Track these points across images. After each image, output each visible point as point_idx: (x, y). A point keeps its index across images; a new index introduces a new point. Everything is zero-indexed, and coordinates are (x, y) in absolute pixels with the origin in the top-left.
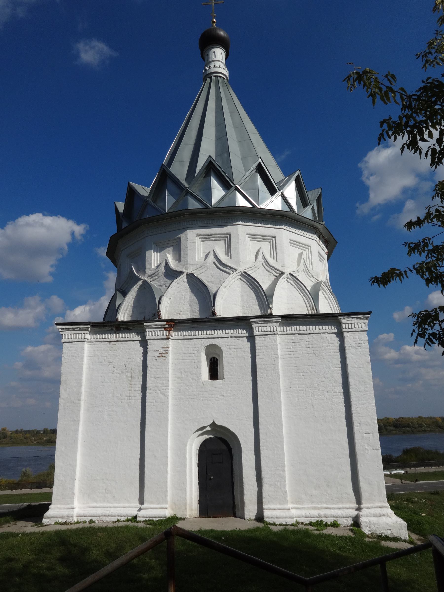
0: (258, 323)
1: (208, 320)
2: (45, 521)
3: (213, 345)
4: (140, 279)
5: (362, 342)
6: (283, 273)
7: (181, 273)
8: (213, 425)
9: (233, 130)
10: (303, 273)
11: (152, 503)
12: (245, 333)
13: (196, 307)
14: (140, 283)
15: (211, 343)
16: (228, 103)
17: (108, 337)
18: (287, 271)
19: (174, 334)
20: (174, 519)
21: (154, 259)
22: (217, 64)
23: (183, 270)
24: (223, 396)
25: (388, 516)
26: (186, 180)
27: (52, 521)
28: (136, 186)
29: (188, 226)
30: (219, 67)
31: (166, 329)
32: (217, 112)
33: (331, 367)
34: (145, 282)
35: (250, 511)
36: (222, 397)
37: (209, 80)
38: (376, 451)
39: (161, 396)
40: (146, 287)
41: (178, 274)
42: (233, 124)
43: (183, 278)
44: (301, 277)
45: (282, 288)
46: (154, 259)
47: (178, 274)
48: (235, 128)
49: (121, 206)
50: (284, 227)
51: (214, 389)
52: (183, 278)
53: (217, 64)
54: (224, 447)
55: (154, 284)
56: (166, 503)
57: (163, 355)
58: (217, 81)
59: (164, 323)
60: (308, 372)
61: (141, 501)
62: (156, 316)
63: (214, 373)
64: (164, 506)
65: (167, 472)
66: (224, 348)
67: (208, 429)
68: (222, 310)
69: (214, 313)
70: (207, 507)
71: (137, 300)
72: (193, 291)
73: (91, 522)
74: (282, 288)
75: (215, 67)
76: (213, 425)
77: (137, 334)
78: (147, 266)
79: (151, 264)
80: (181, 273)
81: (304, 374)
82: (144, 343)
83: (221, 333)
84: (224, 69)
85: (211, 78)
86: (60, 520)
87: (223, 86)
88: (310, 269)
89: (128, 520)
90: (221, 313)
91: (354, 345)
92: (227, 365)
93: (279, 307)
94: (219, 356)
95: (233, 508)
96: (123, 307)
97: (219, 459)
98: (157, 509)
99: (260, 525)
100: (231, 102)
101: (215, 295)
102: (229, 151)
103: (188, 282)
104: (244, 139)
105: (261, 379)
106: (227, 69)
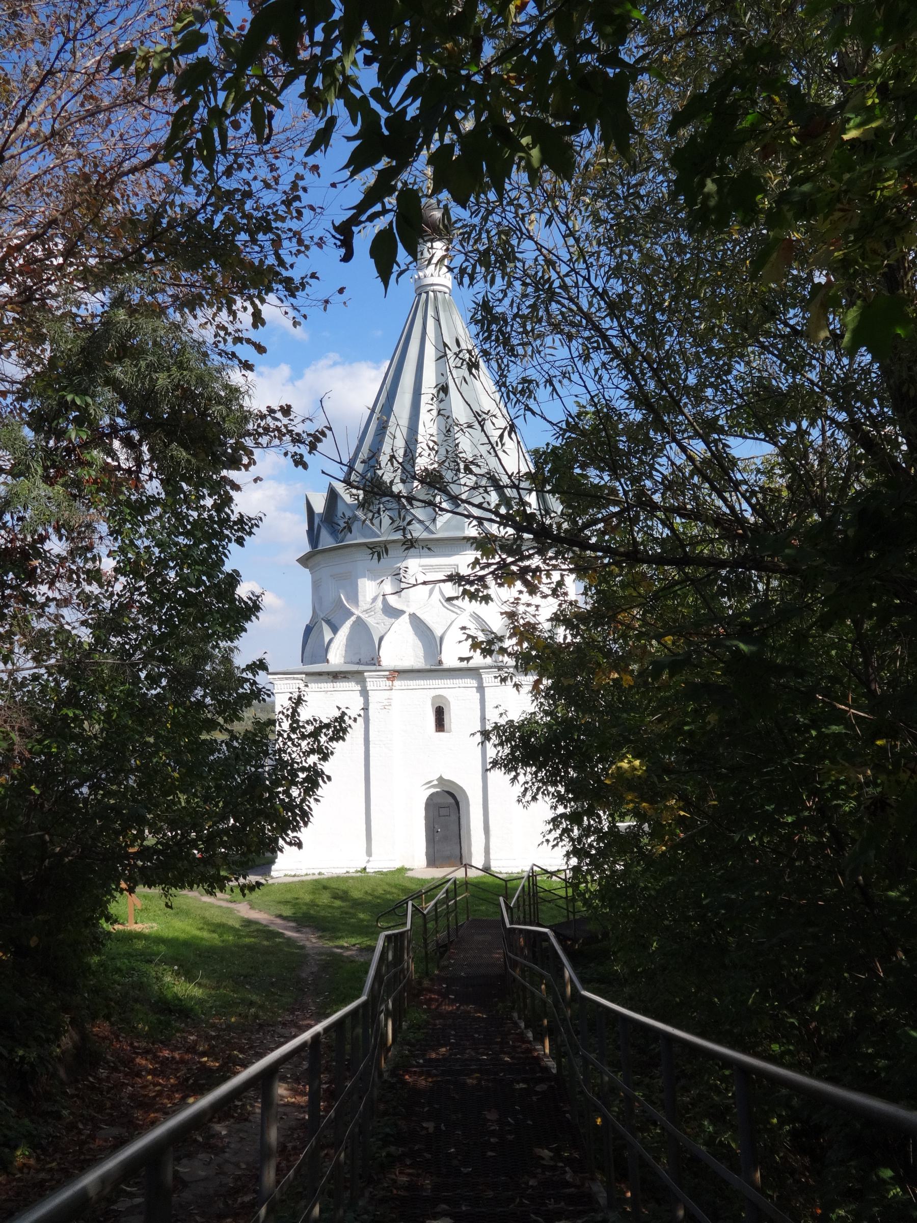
0: (488, 673)
1: (435, 670)
2: (272, 874)
3: (439, 696)
4: (353, 614)
7: (403, 612)
8: (441, 779)
12: (474, 683)
13: (421, 653)
14: (353, 618)
17: (323, 685)
19: (397, 683)
20: (402, 870)
21: (368, 588)
23: (404, 609)
27: (281, 874)
29: (498, 881)
34: (359, 618)
35: (478, 860)
37: (424, 296)
40: (361, 626)
41: (400, 613)
43: (405, 618)
46: (368, 588)
47: (400, 613)
52: (405, 618)
54: (452, 801)
55: (370, 621)
58: (436, 297)
61: (369, 853)
62: (375, 661)
63: (440, 725)
67: (436, 782)
69: (440, 663)
70: (433, 860)
71: (350, 639)
72: (416, 634)
73: (320, 874)
76: (441, 779)
77: (357, 683)
78: (360, 598)
79: (365, 596)
80: (403, 612)
82: (365, 693)
83: (449, 683)
85: (427, 293)
86: (289, 873)
89: (357, 872)
92: (453, 718)
95: (461, 860)
96: (333, 646)
98: (384, 860)
101: (442, 639)
103: (411, 622)
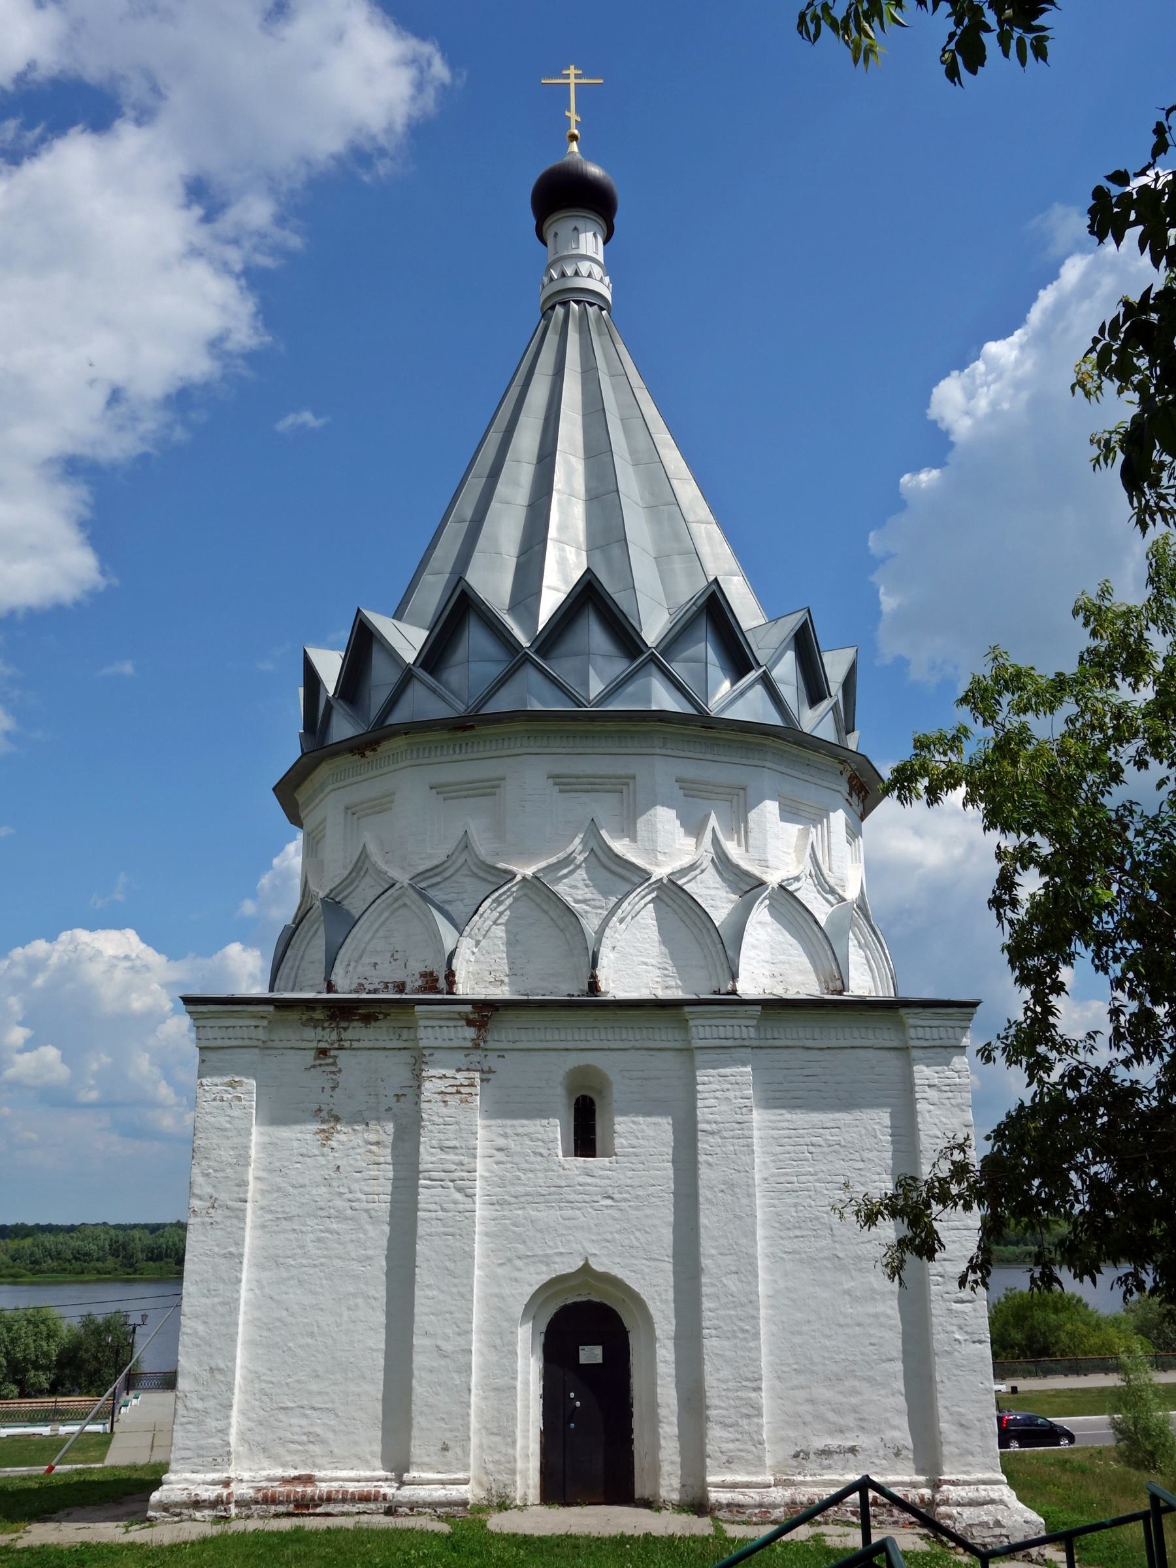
5: (956, 1075)
6: (762, 884)
9: (631, 470)
10: (809, 880)
11: (430, 1467)
15: (582, 1063)
16: (614, 387)
18: (773, 879)
22: (584, 267)
24: (612, 1198)
25: (1002, 1502)
26: (513, 608)
28: (383, 624)
30: (590, 276)
31: (470, 1023)
32: (586, 415)
33: (878, 1133)
36: (609, 1202)
37: (560, 310)
38: (978, 1345)
39: (458, 1196)
42: (631, 454)
44: (808, 895)
45: (760, 923)
48: (636, 464)
49: (330, 666)
50: (768, 764)
51: (589, 1180)
53: (584, 267)
56: (466, 1468)
57: (462, 1090)
59: (468, 1008)
60: (822, 1143)
64: (460, 1476)
65: (470, 1390)
66: (614, 1077)
68: (618, 982)
69: (594, 987)
74: (760, 923)
75: (577, 274)
81: (812, 1149)
84: (601, 280)
85: (565, 304)
87: (600, 334)
88: (825, 871)
90: (612, 985)
91: (936, 1081)
93: (753, 981)
94: (600, 1093)
95: (617, 1483)
97: (589, 1353)
99: (701, 1526)
100: (619, 366)
102: (625, 539)
104: (662, 502)
105: (709, 1158)
106: (607, 280)
